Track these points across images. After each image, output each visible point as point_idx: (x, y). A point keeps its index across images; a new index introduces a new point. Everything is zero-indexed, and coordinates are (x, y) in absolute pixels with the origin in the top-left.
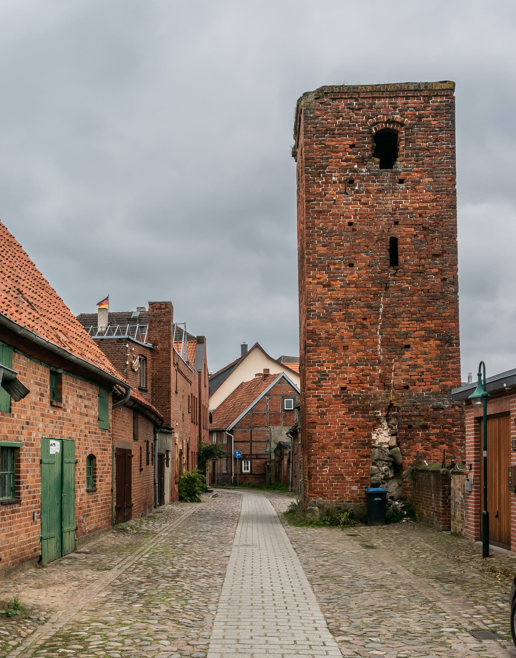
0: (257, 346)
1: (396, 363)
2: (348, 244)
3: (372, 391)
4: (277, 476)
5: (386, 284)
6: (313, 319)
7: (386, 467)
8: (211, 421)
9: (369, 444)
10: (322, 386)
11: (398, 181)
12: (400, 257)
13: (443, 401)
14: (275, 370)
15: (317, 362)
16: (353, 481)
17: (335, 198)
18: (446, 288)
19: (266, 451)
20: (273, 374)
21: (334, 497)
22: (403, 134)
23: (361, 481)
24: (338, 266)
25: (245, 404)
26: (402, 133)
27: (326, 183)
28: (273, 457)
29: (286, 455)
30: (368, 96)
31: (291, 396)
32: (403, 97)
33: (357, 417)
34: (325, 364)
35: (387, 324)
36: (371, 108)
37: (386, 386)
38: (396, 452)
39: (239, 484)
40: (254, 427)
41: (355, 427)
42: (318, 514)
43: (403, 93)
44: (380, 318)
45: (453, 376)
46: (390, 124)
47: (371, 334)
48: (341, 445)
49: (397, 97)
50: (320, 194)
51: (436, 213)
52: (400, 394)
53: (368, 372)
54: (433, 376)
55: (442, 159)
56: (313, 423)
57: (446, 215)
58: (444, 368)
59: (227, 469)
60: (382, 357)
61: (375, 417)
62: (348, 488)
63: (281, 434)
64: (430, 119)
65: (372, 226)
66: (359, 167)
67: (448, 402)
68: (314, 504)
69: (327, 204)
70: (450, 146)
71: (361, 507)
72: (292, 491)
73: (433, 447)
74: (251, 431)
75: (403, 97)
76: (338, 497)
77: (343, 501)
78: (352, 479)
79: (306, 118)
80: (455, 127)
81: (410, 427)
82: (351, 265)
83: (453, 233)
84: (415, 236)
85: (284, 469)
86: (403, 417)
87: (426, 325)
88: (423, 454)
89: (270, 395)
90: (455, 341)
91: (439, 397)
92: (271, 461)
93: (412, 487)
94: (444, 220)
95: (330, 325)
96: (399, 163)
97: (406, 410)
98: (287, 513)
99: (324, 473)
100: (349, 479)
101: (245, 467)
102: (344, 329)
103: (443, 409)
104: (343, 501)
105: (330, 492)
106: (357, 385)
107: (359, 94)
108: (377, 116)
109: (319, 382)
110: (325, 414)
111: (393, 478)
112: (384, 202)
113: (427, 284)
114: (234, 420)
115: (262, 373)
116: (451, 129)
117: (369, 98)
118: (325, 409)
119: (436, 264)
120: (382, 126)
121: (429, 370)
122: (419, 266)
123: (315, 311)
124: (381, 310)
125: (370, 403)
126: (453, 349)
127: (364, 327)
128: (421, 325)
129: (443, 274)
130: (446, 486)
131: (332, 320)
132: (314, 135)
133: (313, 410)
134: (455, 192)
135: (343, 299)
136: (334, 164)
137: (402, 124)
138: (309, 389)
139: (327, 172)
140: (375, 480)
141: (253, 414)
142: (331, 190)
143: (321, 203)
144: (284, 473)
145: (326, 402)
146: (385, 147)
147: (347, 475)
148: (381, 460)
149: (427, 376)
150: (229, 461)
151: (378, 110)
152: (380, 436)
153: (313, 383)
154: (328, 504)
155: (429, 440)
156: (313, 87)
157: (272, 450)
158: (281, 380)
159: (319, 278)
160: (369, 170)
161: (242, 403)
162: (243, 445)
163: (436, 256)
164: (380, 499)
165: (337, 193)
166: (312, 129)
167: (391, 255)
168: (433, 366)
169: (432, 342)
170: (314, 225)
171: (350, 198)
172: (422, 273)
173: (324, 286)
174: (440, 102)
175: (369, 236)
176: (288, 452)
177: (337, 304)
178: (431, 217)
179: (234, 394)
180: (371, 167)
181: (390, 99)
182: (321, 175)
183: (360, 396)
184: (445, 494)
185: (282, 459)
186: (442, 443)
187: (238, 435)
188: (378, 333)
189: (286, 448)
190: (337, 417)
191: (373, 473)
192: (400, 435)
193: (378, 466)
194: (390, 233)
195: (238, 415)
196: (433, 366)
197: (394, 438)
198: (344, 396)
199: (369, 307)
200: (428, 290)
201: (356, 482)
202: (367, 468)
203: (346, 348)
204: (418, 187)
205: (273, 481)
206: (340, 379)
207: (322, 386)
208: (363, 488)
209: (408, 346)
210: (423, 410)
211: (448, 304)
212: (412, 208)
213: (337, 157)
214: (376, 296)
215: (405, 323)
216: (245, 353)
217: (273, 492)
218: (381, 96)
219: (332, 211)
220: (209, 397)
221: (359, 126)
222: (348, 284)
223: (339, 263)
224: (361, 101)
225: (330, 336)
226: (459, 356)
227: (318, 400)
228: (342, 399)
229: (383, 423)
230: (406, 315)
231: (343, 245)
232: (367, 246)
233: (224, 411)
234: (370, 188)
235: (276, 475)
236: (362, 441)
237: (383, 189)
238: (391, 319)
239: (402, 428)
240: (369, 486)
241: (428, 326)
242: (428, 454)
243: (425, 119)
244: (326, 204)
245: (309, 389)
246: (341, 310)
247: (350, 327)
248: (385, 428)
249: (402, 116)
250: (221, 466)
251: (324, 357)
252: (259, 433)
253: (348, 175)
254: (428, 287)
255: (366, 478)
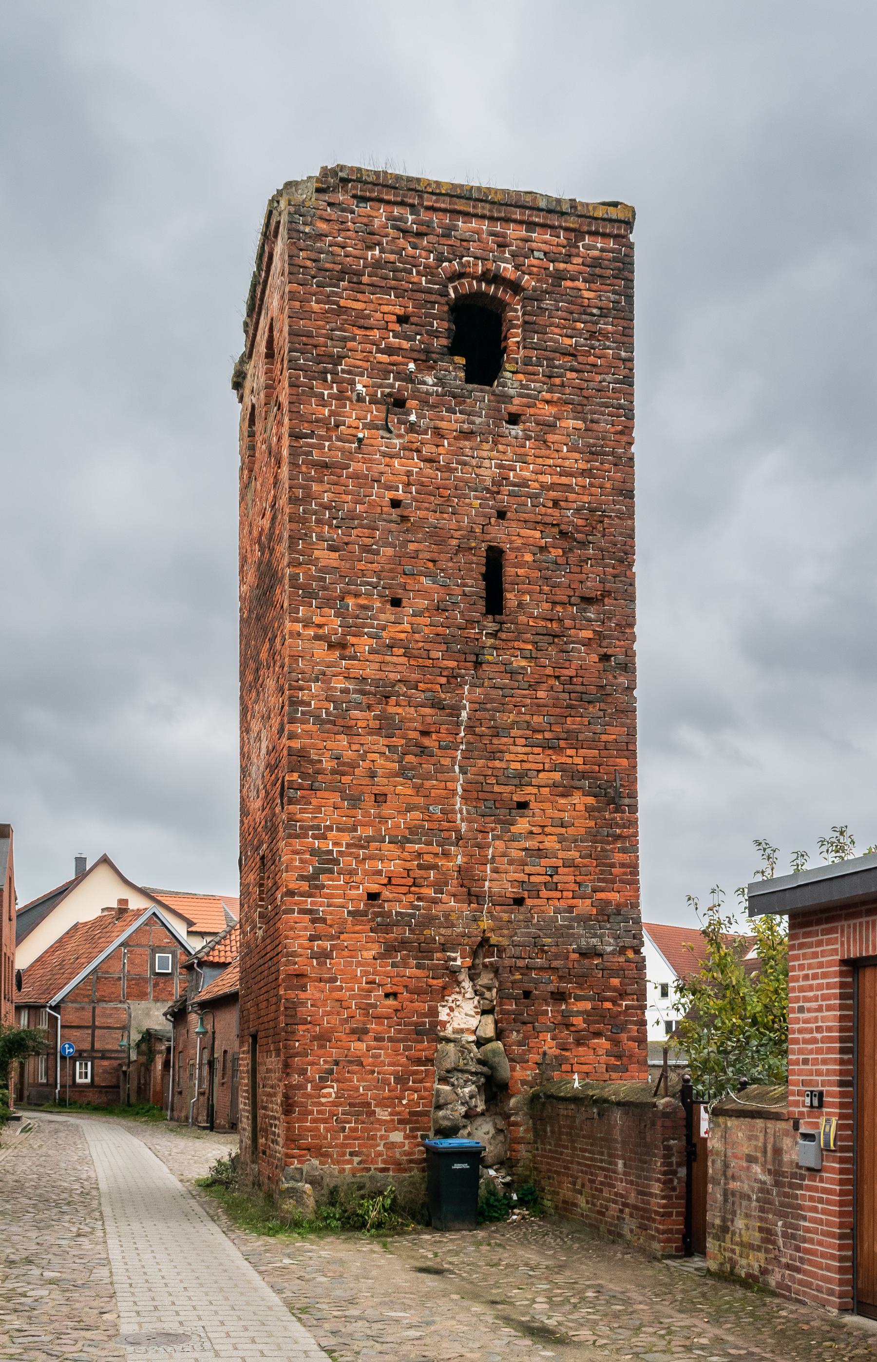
0: (105, 860)
1: (497, 842)
2: (389, 551)
3: (441, 907)
4: (142, 1090)
5: (477, 655)
6: (304, 722)
7: (473, 1087)
8: (19, 988)
9: (430, 1031)
10: (323, 887)
11: (507, 417)
12: (509, 595)
13: (601, 937)
14: (136, 903)
15: (312, 828)
16: (393, 1120)
17: (361, 435)
18: (610, 677)
19: (121, 1046)
20: (135, 908)
21: (348, 1157)
22: (516, 312)
23: (412, 1121)
24: (365, 602)
25: (83, 960)
26: (516, 311)
27: (341, 397)
28: (134, 1056)
29: (160, 1052)
30: (443, 206)
31: (167, 949)
32: (521, 222)
33: (406, 966)
34: (331, 835)
35: (476, 749)
36: (448, 236)
37: (473, 897)
38: (494, 1052)
39: (70, 1104)
40: (99, 1001)
41: (400, 989)
42: (311, 1202)
43: (521, 214)
44: (462, 734)
45: (622, 881)
46: (489, 283)
47: (441, 769)
48: (365, 1031)
49: (507, 220)
50: (324, 422)
51: (589, 503)
52: (505, 916)
53: (429, 858)
54: (578, 879)
55: (604, 381)
56: (300, 976)
57: (613, 511)
58: (602, 861)
59: (47, 1074)
60: (464, 827)
61: (447, 968)
62: (381, 1137)
63: (153, 1016)
64: (580, 284)
65: (445, 516)
66: (419, 369)
67: (612, 941)
68: (298, 1176)
69: (342, 450)
70: (623, 354)
71: (413, 1184)
72: (172, 1119)
73: (579, 1043)
74: (94, 1008)
75: (521, 222)
76: (356, 1159)
77: (369, 1169)
78: (391, 1114)
79: (294, 234)
80: (632, 312)
81: (527, 994)
82: (396, 603)
83: (626, 554)
84: (543, 549)
85: (155, 1078)
86: (512, 969)
87: (564, 760)
88: (556, 1057)
89: (130, 946)
90: (627, 801)
91: (592, 927)
92: (130, 1063)
93: (530, 1136)
94: (606, 520)
95: (344, 740)
96: (509, 375)
97: (518, 954)
98: (208, 1186)
99: (323, 1100)
100: (383, 1114)
101: (81, 1073)
102: (378, 755)
103: (601, 955)
104: (369, 1169)
105: (336, 1146)
106: (404, 889)
107: (421, 197)
108: (461, 257)
109: (315, 876)
110: (329, 956)
111: (482, 1114)
112: (474, 462)
113: (567, 664)
114: (62, 988)
115: (116, 906)
116: (623, 312)
117: (445, 211)
118: (328, 944)
119: (589, 620)
120: (471, 285)
121: (569, 864)
122: (551, 620)
123: (309, 705)
124: (464, 714)
125: (439, 935)
126: (622, 819)
127: (423, 751)
128: (554, 757)
129: (605, 643)
130: (672, 1142)
131: (348, 730)
132: (314, 277)
133: (301, 946)
134: (631, 459)
135: (376, 682)
136: (360, 356)
137: (515, 287)
138: (291, 893)
139: (343, 371)
140: (449, 1119)
141: (98, 978)
142: (351, 415)
143: (327, 444)
144: (154, 1086)
145: (331, 926)
146: (477, 335)
147: (381, 1104)
148: (462, 1071)
149: (566, 877)
150: (51, 1063)
151: (465, 244)
152: (456, 1013)
153: (302, 878)
154: (332, 1176)
155: (568, 1026)
156: (307, 168)
157: (133, 1044)
158: (150, 919)
159: (320, 626)
160: (440, 382)
161: (77, 958)
162: (78, 1034)
163: (588, 600)
164: (466, 1166)
165: (365, 426)
166: (309, 263)
167: (488, 589)
168: (578, 854)
169: (579, 800)
170: (309, 496)
171: (397, 441)
172: (555, 636)
173: (331, 646)
174: (602, 250)
175: (438, 537)
176: (163, 1047)
177: (363, 693)
178: (578, 510)
179: (61, 943)
180: (445, 376)
181: (493, 223)
182: (329, 377)
183: (412, 916)
184: (670, 1164)
185: (151, 1060)
186: (598, 1034)
187: (69, 1015)
188: (457, 768)
189: (161, 1040)
190: (359, 964)
191: (442, 1101)
192: (503, 1012)
193: (453, 1085)
194: (488, 537)
195: (70, 979)
196: (578, 854)
197: (489, 1019)
198: (377, 915)
199: (437, 704)
200: (571, 677)
201: (400, 1122)
202: (426, 1089)
203: (380, 798)
204: (550, 437)
205: (133, 1100)
206: (366, 873)
207: (323, 887)
208: (416, 1137)
209: (523, 806)
210: (556, 957)
211: (612, 714)
212: (537, 485)
213: (366, 340)
214: (452, 680)
215: (520, 749)
216: (82, 873)
217: (135, 1120)
218: (471, 210)
219: (354, 467)
220: (17, 946)
221: (418, 273)
222: (388, 646)
223: (369, 595)
224: (424, 216)
225: (343, 767)
226: (636, 835)
227: (313, 921)
228: (369, 921)
229: (463, 984)
230: (520, 733)
231: (377, 553)
232: (434, 561)
233: (42, 971)
234: (443, 424)
235: (139, 1088)
236: (416, 1024)
237: (472, 433)
238: (486, 741)
239: (510, 997)
240: (431, 1134)
241: (569, 760)
242: (567, 1059)
243: (569, 283)
244: (339, 449)
245: (291, 893)
246: (369, 707)
247: (392, 748)
248: (468, 996)
249: (517, 267)
250: (36, 1070)
251: (328, 817)
252: (107, 1014)
253: (392, 386)
254: (572, 672)
255: (426, 1114)
